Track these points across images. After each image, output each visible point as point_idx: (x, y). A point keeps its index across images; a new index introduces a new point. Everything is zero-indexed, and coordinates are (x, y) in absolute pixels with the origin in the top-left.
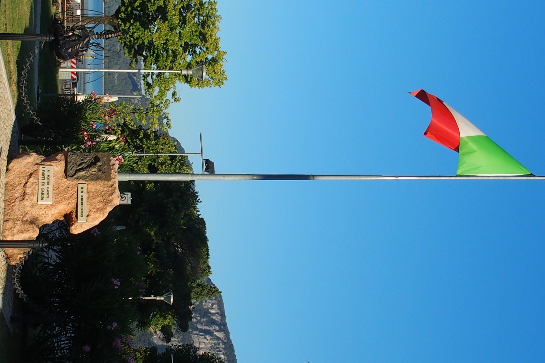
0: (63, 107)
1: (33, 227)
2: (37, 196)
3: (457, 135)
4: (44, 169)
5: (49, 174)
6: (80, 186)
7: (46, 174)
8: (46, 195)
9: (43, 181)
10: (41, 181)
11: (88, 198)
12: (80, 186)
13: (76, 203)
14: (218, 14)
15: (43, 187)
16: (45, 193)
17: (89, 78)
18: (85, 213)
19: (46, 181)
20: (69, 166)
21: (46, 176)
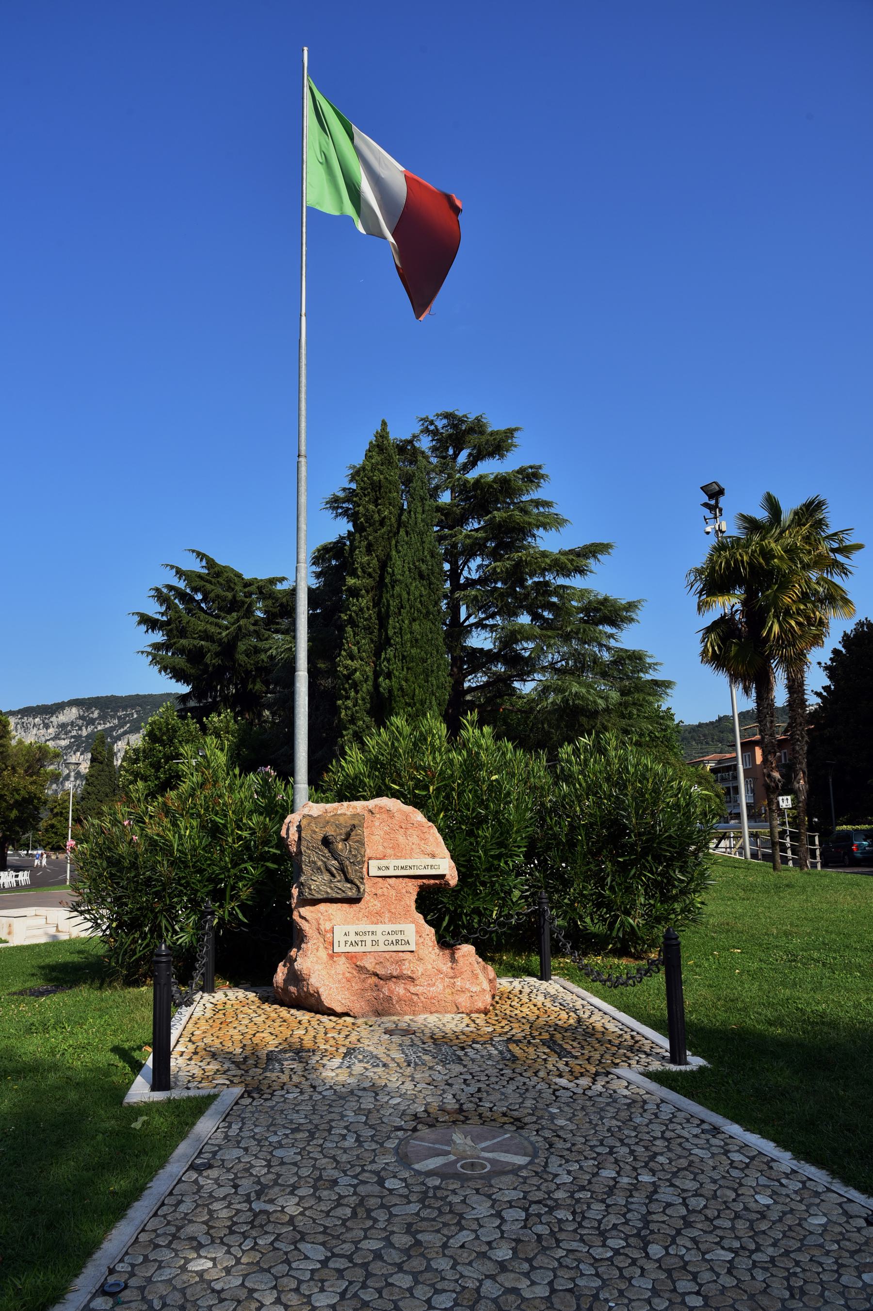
0: (567, 663)
1: (464, 956)
2: (401, 954)
3: (410, 174)
4: (342, 944)
5: (352, 934)
6: (373, 872)
7: (352, 938)
8: (399, 937)
9: (369, 943)
10: (369, 948)
11: (397, 857)
12: (373, 872)
13: (407, 880)
14: (472, 417)
15: (381, 943)
16: (393, 938)
17: (61, 856)
18: (430, 861)
19: (369, 938)
20: (335, 895)
21: (358, 938)
